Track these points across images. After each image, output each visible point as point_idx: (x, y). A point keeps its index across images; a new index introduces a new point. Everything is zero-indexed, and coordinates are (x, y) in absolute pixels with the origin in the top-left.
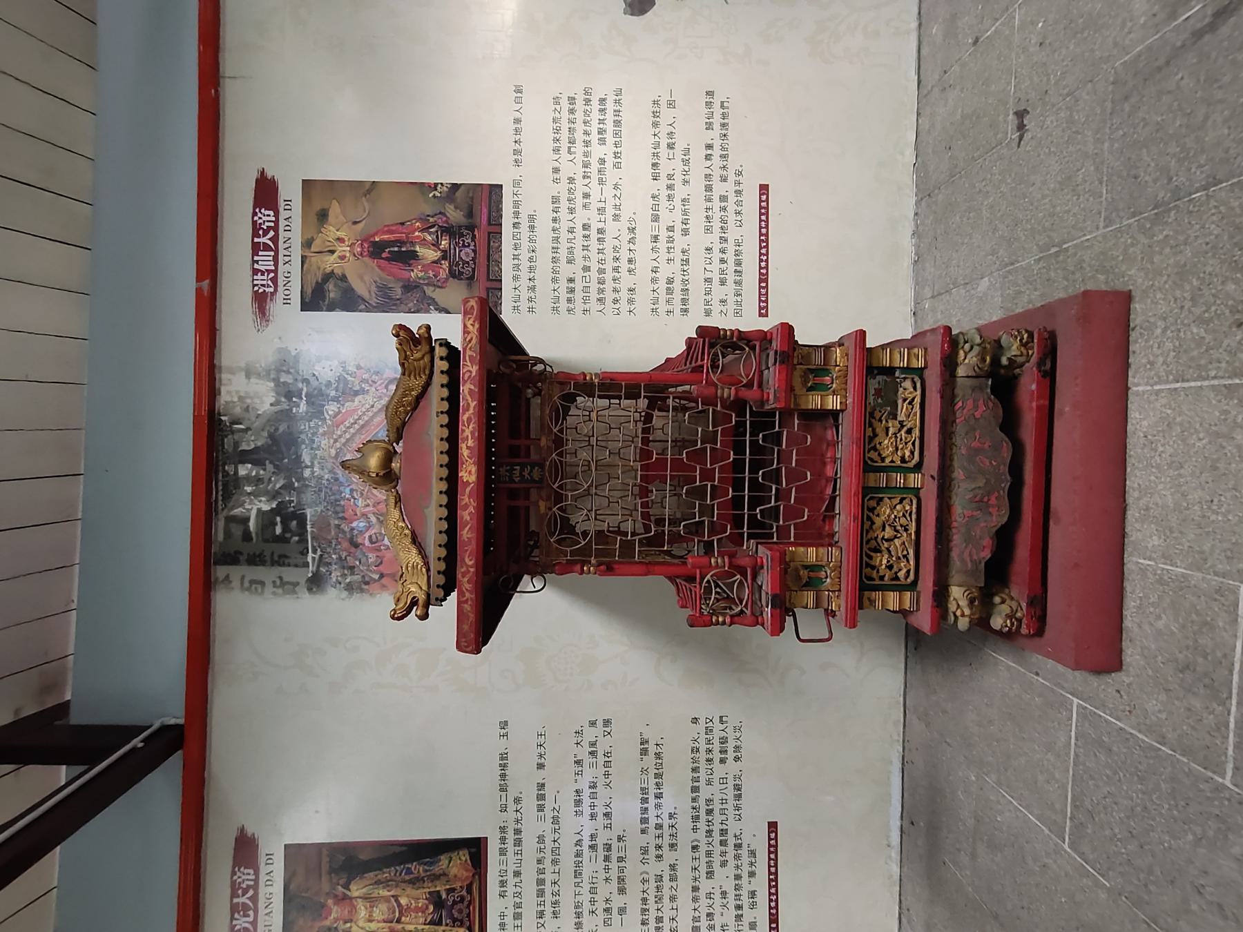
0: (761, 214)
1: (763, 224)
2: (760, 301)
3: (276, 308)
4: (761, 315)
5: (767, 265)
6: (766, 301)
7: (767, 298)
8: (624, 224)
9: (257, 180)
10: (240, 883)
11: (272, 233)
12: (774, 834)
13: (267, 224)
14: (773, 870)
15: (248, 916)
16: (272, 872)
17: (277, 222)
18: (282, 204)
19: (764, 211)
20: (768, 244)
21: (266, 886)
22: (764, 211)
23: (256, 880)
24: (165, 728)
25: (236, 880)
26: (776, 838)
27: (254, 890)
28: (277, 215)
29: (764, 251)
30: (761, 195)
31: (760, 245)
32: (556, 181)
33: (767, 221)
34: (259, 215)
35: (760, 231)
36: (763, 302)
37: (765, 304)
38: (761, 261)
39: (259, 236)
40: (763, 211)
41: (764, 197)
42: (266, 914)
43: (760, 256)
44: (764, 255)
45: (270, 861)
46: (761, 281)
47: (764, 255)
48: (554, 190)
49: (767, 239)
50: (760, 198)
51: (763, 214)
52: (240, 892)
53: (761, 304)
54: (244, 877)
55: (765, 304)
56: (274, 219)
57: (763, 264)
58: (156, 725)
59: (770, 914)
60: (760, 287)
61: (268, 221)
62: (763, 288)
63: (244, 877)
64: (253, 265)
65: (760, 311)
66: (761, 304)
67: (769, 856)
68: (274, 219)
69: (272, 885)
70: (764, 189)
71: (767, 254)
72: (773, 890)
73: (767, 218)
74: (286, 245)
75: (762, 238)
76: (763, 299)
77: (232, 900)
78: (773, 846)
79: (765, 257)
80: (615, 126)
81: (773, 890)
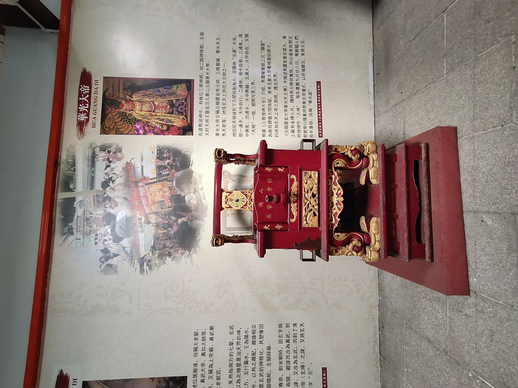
0: (318, 94)
2: (319, 130)
3: (88, 128)
5: (321, 115)
6: (322, 131)
7: (322, 129)
8: (265, 346)
9: (58, 376)
10: (83, 92)
11: (88, 96)
13: (86, 92)
15: (86, 106)
17: (90, 91)
26: (320, 88)
30: (317, 86)
33: (320, 97)
34: (82, 88)
36: (320, 131)
37: (321, 132)
38: (319, 113)
39: (82, 97)
40: (324, 382)
41: (319, 87)
43: (318, 111)
46: (319, 122)
47: (320, 111)
49: (321, 104)
51: (319, 94)
54: (84, 89)
55: (321, 132)
56: (89, 90)
57: (320, 115)
59: (319, 119)
60: (319, 125)
61: (86, 91)
62: (320, 125)
63: (84, 89)
64: (78, 108)
67: (317, 95)
68: (89, 90)
73: (321, 95)
76: (320, 130)
78: (319, 91)
79: (320, 112)
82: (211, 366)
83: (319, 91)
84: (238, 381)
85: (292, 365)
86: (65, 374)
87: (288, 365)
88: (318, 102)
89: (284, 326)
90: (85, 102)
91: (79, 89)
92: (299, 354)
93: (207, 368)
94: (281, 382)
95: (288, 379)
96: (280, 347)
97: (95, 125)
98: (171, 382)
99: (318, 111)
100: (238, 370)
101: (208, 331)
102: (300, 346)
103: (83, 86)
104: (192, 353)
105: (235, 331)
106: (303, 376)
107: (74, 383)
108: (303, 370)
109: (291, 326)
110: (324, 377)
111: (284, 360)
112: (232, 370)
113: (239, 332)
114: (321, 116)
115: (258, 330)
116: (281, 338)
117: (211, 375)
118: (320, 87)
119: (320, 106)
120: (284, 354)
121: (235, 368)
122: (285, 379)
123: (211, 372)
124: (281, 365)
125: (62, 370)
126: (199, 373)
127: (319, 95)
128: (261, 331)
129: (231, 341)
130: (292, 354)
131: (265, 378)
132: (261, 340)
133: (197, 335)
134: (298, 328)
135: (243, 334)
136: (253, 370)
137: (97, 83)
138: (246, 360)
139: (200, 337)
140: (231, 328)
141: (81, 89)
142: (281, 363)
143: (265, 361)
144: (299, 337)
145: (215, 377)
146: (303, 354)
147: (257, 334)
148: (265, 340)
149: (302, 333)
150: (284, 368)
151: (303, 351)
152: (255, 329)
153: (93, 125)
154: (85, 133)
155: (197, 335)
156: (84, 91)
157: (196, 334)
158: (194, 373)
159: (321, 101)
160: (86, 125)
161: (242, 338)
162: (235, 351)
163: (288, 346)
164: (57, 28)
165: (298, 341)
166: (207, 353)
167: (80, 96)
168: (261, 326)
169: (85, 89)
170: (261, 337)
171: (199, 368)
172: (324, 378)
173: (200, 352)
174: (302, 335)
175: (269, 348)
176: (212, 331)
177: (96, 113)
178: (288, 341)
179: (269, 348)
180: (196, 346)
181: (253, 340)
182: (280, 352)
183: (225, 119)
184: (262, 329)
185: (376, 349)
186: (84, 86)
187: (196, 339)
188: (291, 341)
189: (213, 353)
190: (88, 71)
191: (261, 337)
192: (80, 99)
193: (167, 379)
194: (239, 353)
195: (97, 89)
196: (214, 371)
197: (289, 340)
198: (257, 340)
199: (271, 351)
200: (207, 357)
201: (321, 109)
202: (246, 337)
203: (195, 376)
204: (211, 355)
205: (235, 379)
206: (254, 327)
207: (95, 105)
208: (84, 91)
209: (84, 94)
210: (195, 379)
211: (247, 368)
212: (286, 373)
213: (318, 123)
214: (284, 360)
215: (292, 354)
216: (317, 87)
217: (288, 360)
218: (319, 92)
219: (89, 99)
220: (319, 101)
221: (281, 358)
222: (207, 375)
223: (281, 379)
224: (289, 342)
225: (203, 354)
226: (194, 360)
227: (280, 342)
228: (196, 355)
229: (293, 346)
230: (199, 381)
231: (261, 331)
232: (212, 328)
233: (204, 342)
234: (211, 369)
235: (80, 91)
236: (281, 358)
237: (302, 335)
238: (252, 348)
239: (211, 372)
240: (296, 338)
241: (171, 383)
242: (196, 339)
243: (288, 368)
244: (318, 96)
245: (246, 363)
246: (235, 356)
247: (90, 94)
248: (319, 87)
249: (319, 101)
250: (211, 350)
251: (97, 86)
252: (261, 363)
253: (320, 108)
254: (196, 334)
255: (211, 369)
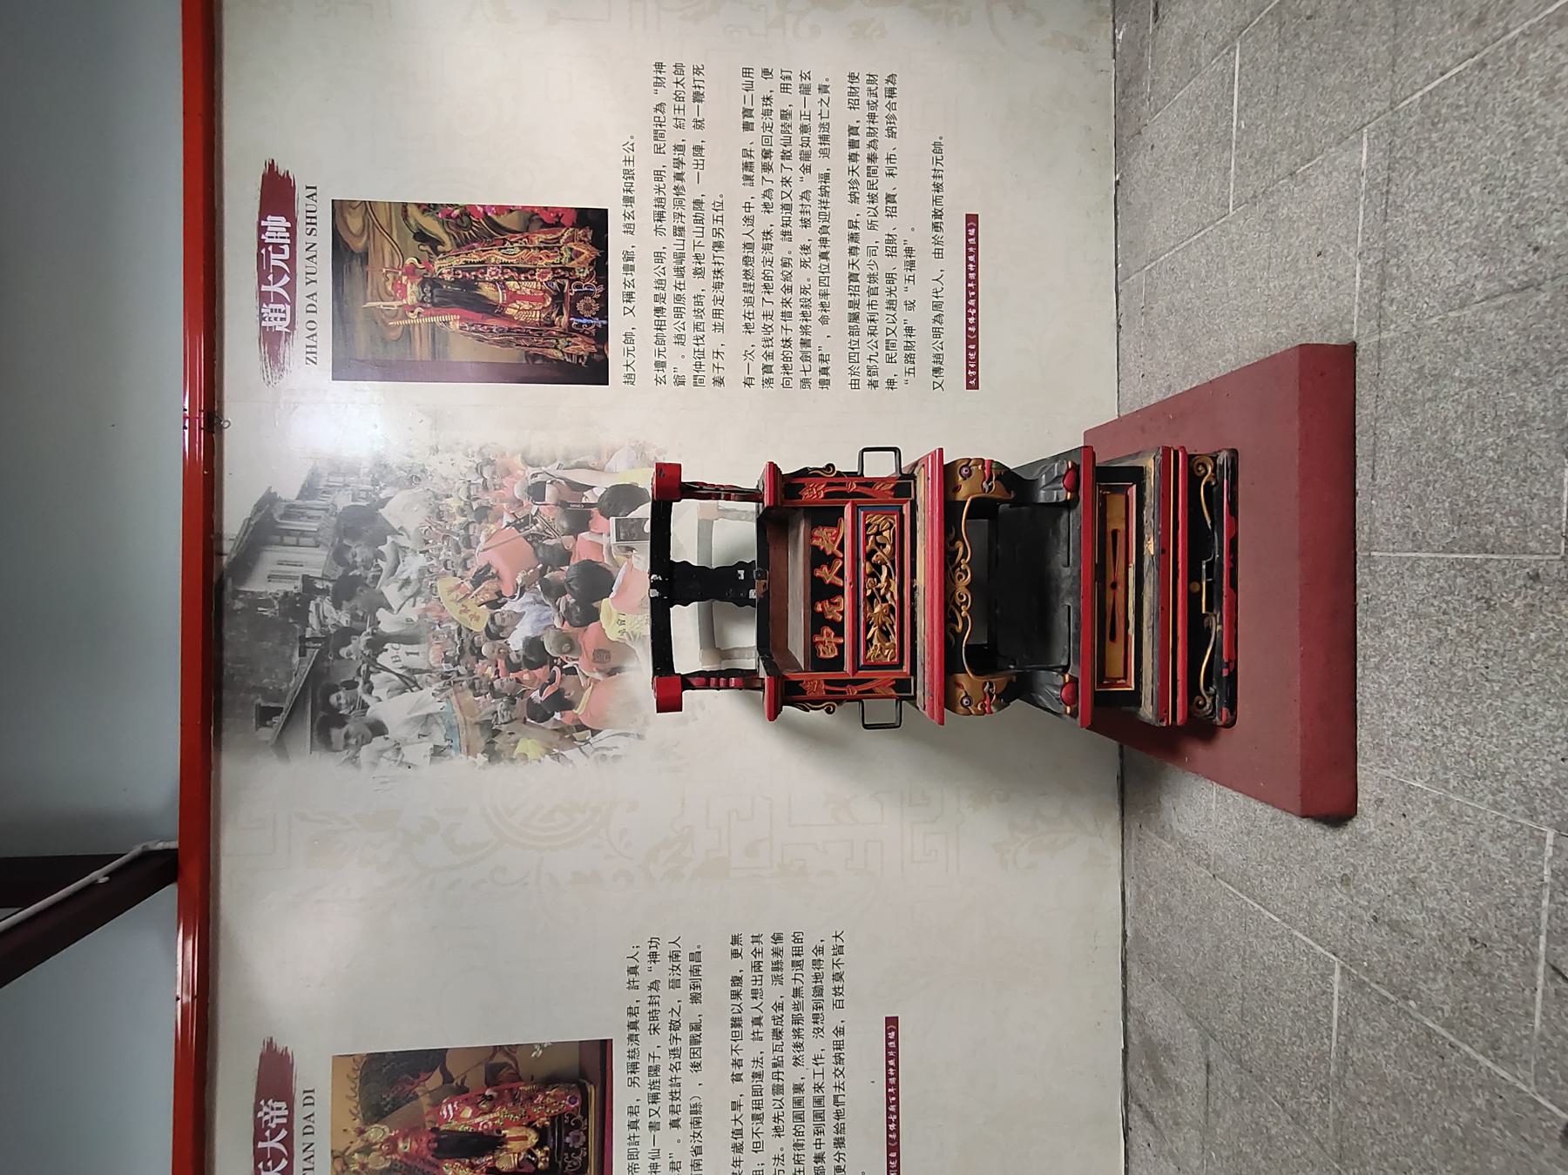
2: (968, 368)
3: (294, 352)
4: (969, 387)
5: (977, 321)
9: (262, 1056)
10: (267, 1122)
11: (283, 1133)
16: (312, 1115)
17: (290, 1117)
18: (299, 1097)
19: (972, 249)
21: (305, 1134)
22: (972, 249)
24: (147, 856)
25: (261, 1118)
27: (287, 1159)
28: (290, 1108)
29: (972, 302)
30: (887, 1031)
32: (632, 985)
33: (976, 263)
34: (265, 1109)
36: (972, 369)
38: (969, 315)
39: (265, 1140)
40: (891, 1053)
41: (972, 232)
42: (305, 1160)
43: (887, 1116)
47: (972, 307)
48: (631, 998)
49: (977, 287)
50: (967, 232)
51: (972, 254)
52: (268, 1133)
53: (970, 372)
54: (272, 1113)
56: (286, 1113)
57: (892, 1126)
58: (137, 850)
60: (968, 350)
61: (278, 1117)
62: (972, 351)
63: (272, 1113)
64: (260, 287)
65: (968, 382)
67: (967, 259)
69: (313, 1133)
70: (972, 220)
73: (977, 258)
76: (972, 366)
77: (255, 1144)
86: (280, 1050)
88: (968, 280)
90: (279, 298)
97: (315, 218)
118: (977, 232)
119: (973, 293)
125: (271, 1039)
127: (971, 258)
137: (311, 1101)
153: (307, 217)
154: (286, 366)
156: (272, 1118)
160: (286, 341)
167: (259, 1136)
169: (275, 1112)
186: (270, 1102)
190: (280, 1050)
192: (264, 288)
195: (312, 1118)
201: (977, 302)
207: (311, 257)
209: (270, 1128)
219: (288, 1142)
235: (257, 1121)
244: (968, 262)
247: (289, 1126)
248: (892, 1035)
249: (972, 276)
251: (308, 1110)
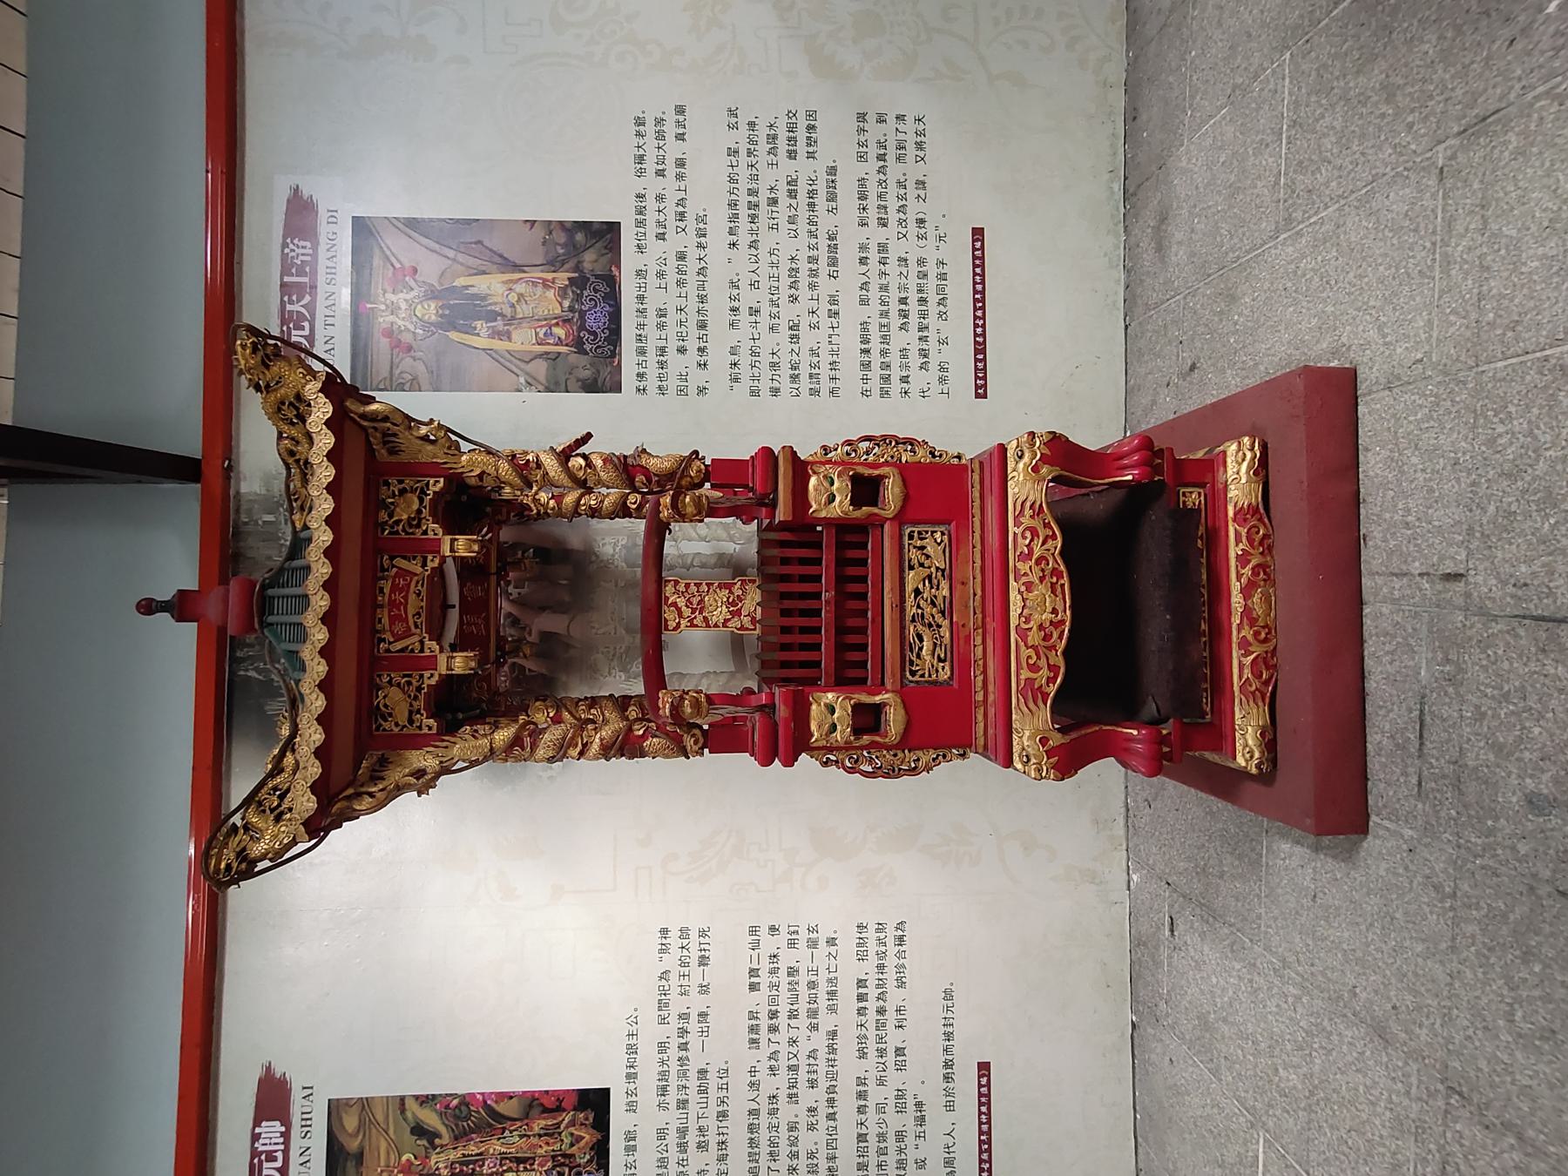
0: (975, 266)
1: (978, 279)
2: (977, 378)
4: (978, 396)
5: (984, 331)
6: (984, 378)
7: (985, 373)
8: (821, 165)
9: (260, 1081)
12: (985, 1079)
13: (301, 258)
14: (985, 1127)
15: (303, 328)
20: (984, 304)
23: (315, 256)
26: (988, 1085)
29: (979, 313)
31: (975, 306)
33: (983, 275)
34: (291, 246)
35: (974, 288)
36: (980, 379)
37: (982, 382)
38: (976, 326)
40: (983, 1100)
41: (978, 245)
43: (980, 1164)
44: (980, 318)
45: (334, 220)
46: (977, 352)
47: (980, 318)
49: (984, 298)
51: (978, 266)
53: (978, 382)
55: (982, 382)
56: (311, 251)
57: (979, 330)
59: (976, 343)
60: (976, 360)
61: (303, 255)
62: (980, 361)
65: (976, 390)
66: (978, 382)
67: (974, 271)
68: (311, 251)
71: (984, 318)
72: (985, 1156)
73: (983, 270)
74: (330, 254)
75: (976, 296)
76: (980, 375)
78: (985, 1095)
79: (982, 322)
80: (792, 382)
81: (985, 1156)
82: (681, 202)
83: (985, 1095)
84: (753, 245)
85: (893, 216)
87: (883, 216)
88: (975, 292)
89: (871, 118)
91: (283, 251)
92: (912, 192)
93: (671, 209)
94: (864, 255)
95: (883, 248)
96: (861, 169)
98: (579, 234)
99: (975, 317)
100: (753, 219)
101: (671, 117)
102: (914, 172)
103: (292, 242)
104: (632, 167)
105: (743, 122)
106: (922, 243)
107: (330, 220)
108: (922, 231)
109: (891, 119)
110: (984, 1086)
111: (873, 202)
112: (736, 216)
113: (752, 125)
114: (984, 335)
115: (802, 123)
116: (865, 149)
117: (682, 225)
118: (989, 1081)
119: (980, 304)
120: (873, 189)
121: (743, 212)
122: (874, 248)
123: (681, 216)
124: (865, 214)
126: (651, 217)
128: (811, 128)
129: (733, 146)
130: (893, 190)
131: (823, 243)
132: (811, 149)
133: (644, 124)
134: (910, 126)
135: (762, 132)
136: (792, 220)
137: (334, 220)
138: (773, 195)
139: (650, 129)
140: (732, 113)
141: (286, 251)
142: (864, 209)
143: (821, 200)
144: (911, 150)
145: (691, 230)
146: (922, 193)
147: (801, 135)
148: (820, 149)
149: (919, 139)
150: (873, 222)
151: (921, 184)
152: (794, 120)
153: (303, 1120)
155: (644, 124)
156: (298, 255)
157: (640, 122)
158: (638, 217)
159: (984, 288)
161: (762, 139)
162: (743, 173)
163: (882, 170)
164: (197, 481)
165: (910, 158)
166: (671, 171)
168: (811, 115)
169: (271, 1130)
170: (810, 142)
171: (651, 204)
172: (984, 1090)
173: (650, 166)
174: (919, 146)
175: (832, 171)
176: (681, 118)
177: (334, 236)
178: (881, 158)
179: (832, 171)
180: (641, 152)
181: (791, 148)
182: (862, 182)
183: (707, 385)
184: (813, 123)
185: (1116, 189)
186: (296, 241)
187: (638, 134)
188: (891, 158)
189: (686, 171)
191: (810, 142)
193: (568, 226)
194: (754, 178)
196: (690, 217)
197: (885, 154)
198: (801, 147)
199: (837, 178)
200: (670, 182)
201: (984, 313)
202: (772, 138)
203: (640, 224)
204: (679, 177)
205: (744, 239)
206: (791, 115)
207: (332, 257)
208: (298, 255)
210: (642, 230)
211: (775, 215)
212: (879, 235)
213: (975, 355)
214: (873, 202)
215: (893, 190)
216: (973, 245)
217: (883, 203)
218: (979, 261)
220: (979, 287)
221: (863, 197)
222: (672, 223)
223: (863, 248)
224: (885, 160)
225: (661, 173)
226: (638, 185)
227: (862, 157)
228: (640, 173)
229: (894, 171)
230: (651, 236)
231: (811, 128)
232: (680, 110)
233: (662, 143)
234: (681, 209)
236: (863, 197)
237: (919, 146)
238: (787, 167)
239: (681, 216)
240: (904, 152)
241: (579, 237)
242: (638, 134)
243: (883, 223)
245: (773, 202)
246: (743, 185)
248: (978, 245)
249: (979, 287)
250: (681, 163)
251: (306, 1143)
252: (812, 206)
253: (980, 308)
254: (640, 122)
255: (681, 209)
